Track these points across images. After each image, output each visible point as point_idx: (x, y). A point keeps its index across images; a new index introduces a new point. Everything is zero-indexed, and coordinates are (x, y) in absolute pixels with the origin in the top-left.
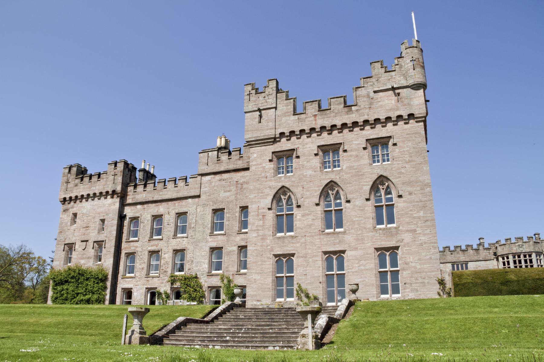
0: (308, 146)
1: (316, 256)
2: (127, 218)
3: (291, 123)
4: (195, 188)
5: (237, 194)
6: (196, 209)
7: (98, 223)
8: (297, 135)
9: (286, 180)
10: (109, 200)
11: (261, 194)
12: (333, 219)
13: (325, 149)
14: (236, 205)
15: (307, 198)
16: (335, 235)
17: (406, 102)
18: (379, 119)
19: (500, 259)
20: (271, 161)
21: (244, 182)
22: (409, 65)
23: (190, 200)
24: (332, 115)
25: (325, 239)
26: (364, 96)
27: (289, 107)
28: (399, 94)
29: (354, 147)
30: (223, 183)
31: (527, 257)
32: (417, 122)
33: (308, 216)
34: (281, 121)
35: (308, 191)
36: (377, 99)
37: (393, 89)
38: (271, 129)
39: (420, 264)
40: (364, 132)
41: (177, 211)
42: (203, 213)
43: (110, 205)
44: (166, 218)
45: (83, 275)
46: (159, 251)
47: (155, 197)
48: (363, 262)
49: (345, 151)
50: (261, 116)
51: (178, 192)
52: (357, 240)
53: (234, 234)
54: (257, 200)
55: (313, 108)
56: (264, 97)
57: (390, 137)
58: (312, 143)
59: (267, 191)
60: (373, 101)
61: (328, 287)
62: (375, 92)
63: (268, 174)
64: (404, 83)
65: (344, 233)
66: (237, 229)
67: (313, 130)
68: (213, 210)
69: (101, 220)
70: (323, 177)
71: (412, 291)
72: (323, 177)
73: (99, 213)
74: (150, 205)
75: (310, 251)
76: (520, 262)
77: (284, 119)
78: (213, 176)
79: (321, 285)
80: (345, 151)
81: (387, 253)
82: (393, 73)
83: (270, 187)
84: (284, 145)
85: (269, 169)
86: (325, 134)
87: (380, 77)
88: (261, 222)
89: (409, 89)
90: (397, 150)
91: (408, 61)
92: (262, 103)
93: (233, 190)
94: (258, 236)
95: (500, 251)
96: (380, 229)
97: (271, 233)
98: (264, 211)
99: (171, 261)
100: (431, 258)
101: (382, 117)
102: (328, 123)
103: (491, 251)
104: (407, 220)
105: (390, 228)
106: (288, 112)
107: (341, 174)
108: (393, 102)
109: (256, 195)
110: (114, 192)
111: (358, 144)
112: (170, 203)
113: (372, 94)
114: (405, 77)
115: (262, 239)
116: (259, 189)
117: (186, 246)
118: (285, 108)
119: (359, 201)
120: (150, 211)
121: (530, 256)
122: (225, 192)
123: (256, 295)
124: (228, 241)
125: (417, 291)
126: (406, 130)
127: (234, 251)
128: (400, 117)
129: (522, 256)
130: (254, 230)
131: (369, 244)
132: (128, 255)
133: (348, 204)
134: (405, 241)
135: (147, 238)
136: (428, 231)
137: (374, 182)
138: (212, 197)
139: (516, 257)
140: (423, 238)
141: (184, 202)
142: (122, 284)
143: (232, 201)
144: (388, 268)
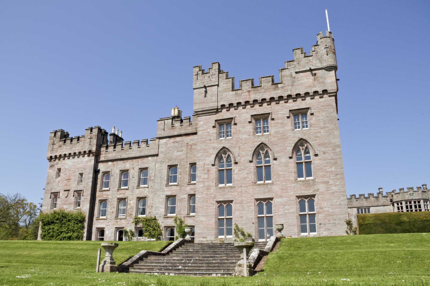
0: (243, 115)
1: (250, 202)
2: (101, 172)
3: (230, 97)
4: (154, 149)
5: (187, 153)
6: (155, 165)
7: (77, 176)
8: (235, 107)
9: (226, 142)
10: (86, 158)
11: (206, 154)
12: (264, 173)
13: (257, 118)
14: (187, 162)
15: (243, 156)
16: (265, 186)
17: (321, 80)
18: (300, 94)
19: (396, 205)
20: (214, 127)
21: (193, 144)
22: (323, 51)
23: (150, 158)
24: (263, 91)
25: (257, 189)
26: (288, 76)
27: (229, 85)
28: (315, 74)
29: (280, 116)
30: (176, 144)
31: (417, 203)
32: (329, 96)
33: (244, 171)
34: (222, 95)
35: (243, 151)
36: (298, 78)
37: (311, 70)
38: (214, 102)
39: (332, 209)
40: (287, 104)
41: (140, 167)
42: (161, 168)
43: (87, 162)
44: (131, 172)
45: (65, 217)
46: (126, 199)
47: (123, 155)
48: (287, 207)
49: (273, 119)
50: (206, 92)
51: (140, 152)
52: (282, 189)
53: (185, 185)
54: (203, 158)
55: (247, 85)
56: (209, 77)
57: (308, 108)
58: (247, 113)
59: (211, 151)
60: (295, 80)
61: (259, 227)
62: (296, 73)
63: (212, 138)
64: (319, 65)
65: (272, 184)
66: (188, 181)
67: (247, 103)
68: (168, 166)
69: (80, 174)
70: (255, 140)
71: (326, 230)
72: (255, 140)
73: (78, 169)
74: (119, 162)
75: (245, 199)
76: (411, 207)
77: (224, 94)
78: (168, 139)
79: (254, 225)
80: (273, 119)
81: (306, 200)
82: (311, 58)
83: (213, 148)
84: (224, 114)
85: (213, 133)
86: (257, 106)
87: (300, 61)
88: (206, 176)
89: (323, 71)
90: (314, 119)
91: (323, 48)
92: (207, 82)
93: (184, 150)
94: (204, 186)
95: (395, 198)
96: (301, 181)
97: (214, 184)
98: (209, 166)
99: (135, 206)
100: (340, 204)
101: (302, 93)
102: (259, 97)
103: (388, 198)
104: (322, 174)
105: (308, 180)
106: (227, 89)
107: (270, 137)
108: (311, 80)
109: (202, 154)
110: (90, 152)
111: (283, 114)
112: (134, 160)
113: (294, 75)
114: (320, 60)
115: (207, 189)
116: (205, 150)
117: (147, 194)
118: (225, 85)
119: (284, 159)
120: (118, 167)
121: (419, 202)
122: (178, 151)
123: (202, 233)
124: (180, 190)
125: (330, 230)
126: (321, 102)
127: (185, 198)
128: (316, 93)
129: (413, 202)
130: (201, 182)
131: (292, 193)
132: (101, 201)
133: (275, 161)
134: (320, 191)
135: (116, 188)
136: (338, 183)
137: (296, 144)
138: (168, 155)
139: (408, 203)
140: (334, 188)
141: (145, 160)
142: (97, 224)
143: (183, 159)
144: (307, 212)
